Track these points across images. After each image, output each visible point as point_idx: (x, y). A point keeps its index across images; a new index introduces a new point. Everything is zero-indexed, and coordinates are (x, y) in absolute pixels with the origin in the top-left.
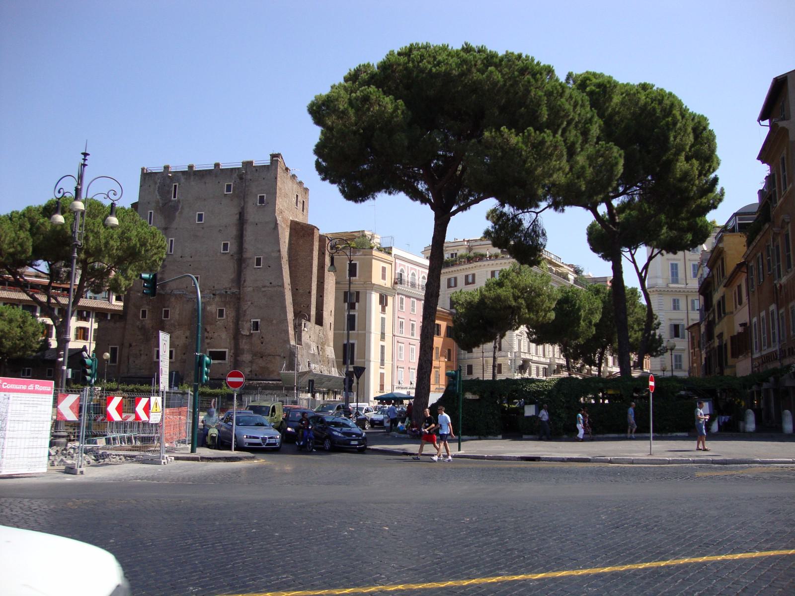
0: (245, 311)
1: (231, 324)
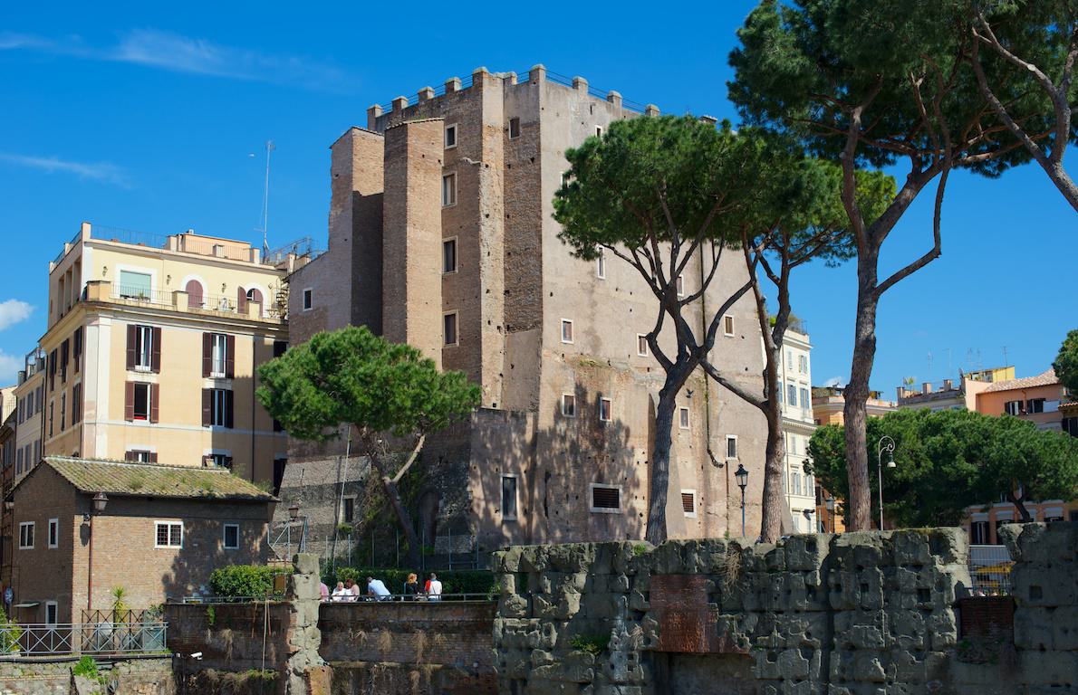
0: (718, 418)
1: (697, 440)
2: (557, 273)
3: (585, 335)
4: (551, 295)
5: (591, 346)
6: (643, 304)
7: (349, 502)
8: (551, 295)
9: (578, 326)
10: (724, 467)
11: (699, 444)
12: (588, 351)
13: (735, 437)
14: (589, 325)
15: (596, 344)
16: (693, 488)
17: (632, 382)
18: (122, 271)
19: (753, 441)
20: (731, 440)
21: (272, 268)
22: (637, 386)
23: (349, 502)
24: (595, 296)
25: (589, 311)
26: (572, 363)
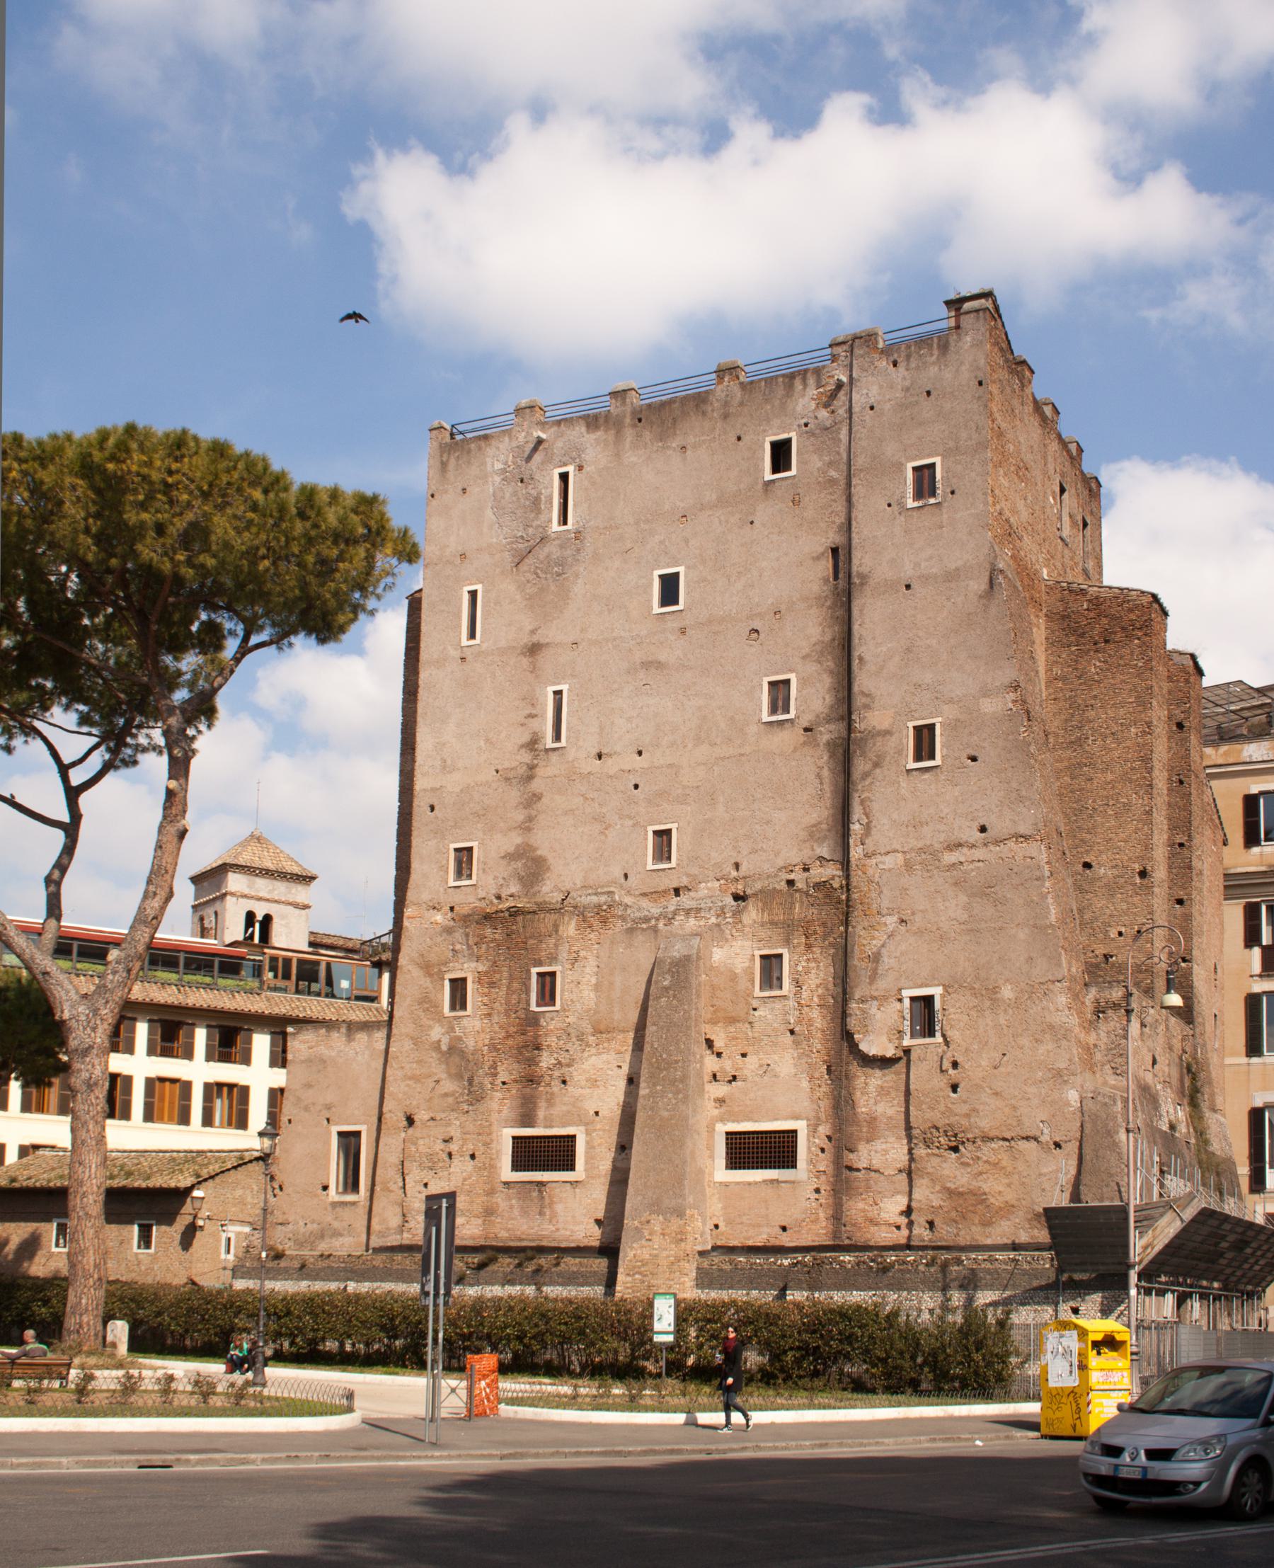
0: (876, 958)
1: (815, 1014)
2: (444, 768)
3: (504, 862)
4: (432, 808)
5: (521, 879)
6: (671, 766)
7: (925, 732)
8: (432, 808)
9: (489, 851)
10: (903, 1063)
11: (819, 1020)
12: (514, 888)
13: (936, 991)
14: (519, 840)
15: (532, 867)
16: (796, 1117)
17: (619, 926)
18: (1253, 1048)
19: (996, 990)
20: (928, 1000)
21: (386, 976)
22: (630, 931)
23: (925, 732)
24: (536, 785)
25: (520, 816)
26: (465, 919)
